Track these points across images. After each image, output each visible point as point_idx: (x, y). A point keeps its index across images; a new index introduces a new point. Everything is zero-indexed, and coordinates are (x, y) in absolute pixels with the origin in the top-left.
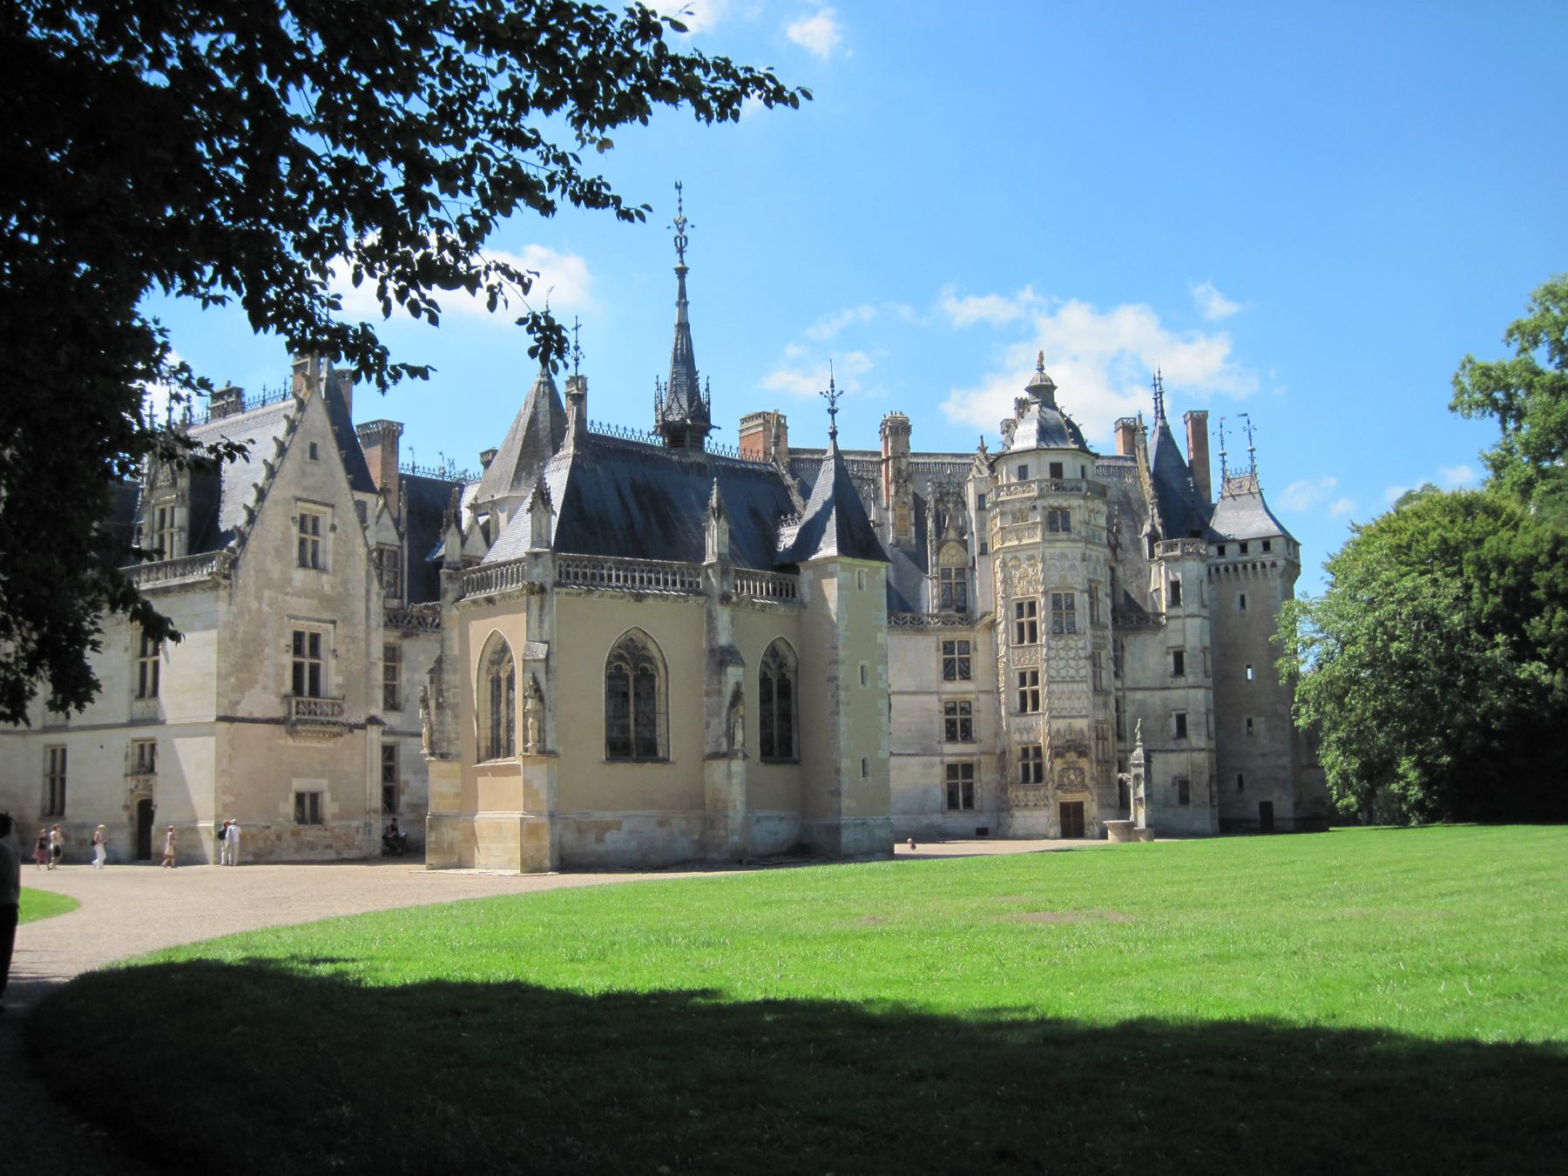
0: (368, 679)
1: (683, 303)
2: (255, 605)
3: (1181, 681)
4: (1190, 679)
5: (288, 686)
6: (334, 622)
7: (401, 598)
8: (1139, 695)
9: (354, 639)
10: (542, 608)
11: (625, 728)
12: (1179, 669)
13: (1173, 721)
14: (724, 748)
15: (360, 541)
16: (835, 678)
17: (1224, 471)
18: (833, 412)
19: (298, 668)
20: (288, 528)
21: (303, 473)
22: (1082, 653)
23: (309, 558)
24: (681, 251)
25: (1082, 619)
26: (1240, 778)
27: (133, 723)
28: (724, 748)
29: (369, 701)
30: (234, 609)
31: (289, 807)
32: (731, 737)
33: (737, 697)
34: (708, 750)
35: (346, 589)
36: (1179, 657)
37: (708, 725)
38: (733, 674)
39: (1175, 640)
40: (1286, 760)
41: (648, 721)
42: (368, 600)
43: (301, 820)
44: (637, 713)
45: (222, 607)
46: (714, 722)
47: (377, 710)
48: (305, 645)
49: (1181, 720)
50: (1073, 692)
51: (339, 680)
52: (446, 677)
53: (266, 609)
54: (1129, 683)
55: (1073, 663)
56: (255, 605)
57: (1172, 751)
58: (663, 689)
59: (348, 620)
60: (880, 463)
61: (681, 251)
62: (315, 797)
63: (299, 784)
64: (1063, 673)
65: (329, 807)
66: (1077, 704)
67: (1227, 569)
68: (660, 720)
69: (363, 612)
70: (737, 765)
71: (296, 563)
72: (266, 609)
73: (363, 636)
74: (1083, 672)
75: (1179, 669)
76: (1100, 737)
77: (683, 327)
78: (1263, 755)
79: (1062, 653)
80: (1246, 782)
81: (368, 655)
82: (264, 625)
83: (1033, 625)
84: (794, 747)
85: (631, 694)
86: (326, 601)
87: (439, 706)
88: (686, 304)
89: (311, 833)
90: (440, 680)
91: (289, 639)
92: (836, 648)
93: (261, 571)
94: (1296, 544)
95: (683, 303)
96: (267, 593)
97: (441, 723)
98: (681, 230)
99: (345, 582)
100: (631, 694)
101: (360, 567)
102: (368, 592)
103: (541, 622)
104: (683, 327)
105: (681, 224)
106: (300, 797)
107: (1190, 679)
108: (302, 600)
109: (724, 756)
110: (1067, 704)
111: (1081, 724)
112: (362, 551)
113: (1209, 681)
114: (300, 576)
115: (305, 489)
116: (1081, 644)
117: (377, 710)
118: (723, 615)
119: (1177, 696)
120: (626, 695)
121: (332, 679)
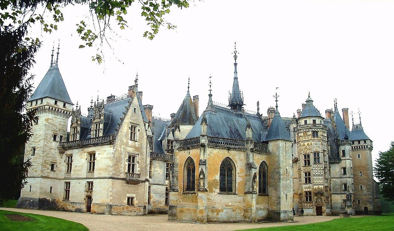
0: (146, 169)
1: (236, 72)
2: (120, 149)
3: (345, 176)
4: (348, 175)
5: (127, 171)
6: (138, 154)
7: (153, 149)
8: (334, 179)
9: (143, 159)
10: (204, 151)
11: (224, 184)
12: (345, 173)
13: (343, 186)
14: (251, 190)
15: (145, 133)
16: (280, 172)
17: (353, 123)
18: (276, 101)
19: (129, 165)
20: (128, 130)
21: (132, 116)
22: (322, 169)
23: (132, 138)
24: (235, 60)
25: (321, 160)
26: (359, 201)
27: (65, 179)
28: (251, 190)
29: (146, 175)
30: (115, 150)
31: (126, 201)
32: (253, 187)
33: (255, 177)
34: (246, 191)
35: (141, 146)
36: (344, 169)
37: (246, 184)
38: (253, 171)
39: (344, 166)
40: (371, 196)
41: (230, 182)
42: (147, 149)
43: (128, 203)
44: (227, 180)
45: (112, 149)
46: (248, 183)
47: (148, 178)
48: (131, 158)
49: (345, 185)
50: (319, 178)
51: (139, 169)
52: (175, 169)
53: (122, 150)
54: (332, 176)
55: (319, 171)
56: (120, 149)
57: (343, 194)
58: (234, 174)
59: (142, 154)
60: (268, 119)
61: (235, 60)
62: (132, 198)
63: (128, 195)
64: (317, 173)
65: (135, 202)
66: (320, 181)
67: (355, 148)
68: (234, 182)
69: (145, 152)
70: (254, 196)
71: (130, 139)
72: (122, 150)
73: (145, 158)
74: (322, 173)
75: (345, 173)
76: (174, 183)
77: (236, 78)
78: (365, 195)
79: (316, 169)
80: (360, 202)
81: (146, 163)
82: (121, 154)
83: (309, 161)
84: (267, 190)
85: (226, 175)
86: (137, 149)
87: (173, 177)
88: (237, 73)
89: (131, 208)
90: (173, 170)
91: (127, 158)
92: (280, 164)
93: (122, 140)
94: (372, 142)
95: (236, 72)
96: (122, 146)
97: (173, 181)
98: (235, 54)
99: (141, 144)
100: (226, 175)
101: (145, 141)
102: (147, 147)
103: (204, 154)
104: (236, 78)
105: (235, 52)
106: (129, 198)
107: (348, 175)
108: (131, 148)
109: (251, 193)
110: (318, 181)
111: (321, 187)
112: (146, 136)
113: (352, 176)
114: (130, 142)
115: (133, 120)
116: (321, 166)
117: (148, 178)
118: (251, 155)
119: (344, 180)
120: (225, 175)
121: (137, 169)
